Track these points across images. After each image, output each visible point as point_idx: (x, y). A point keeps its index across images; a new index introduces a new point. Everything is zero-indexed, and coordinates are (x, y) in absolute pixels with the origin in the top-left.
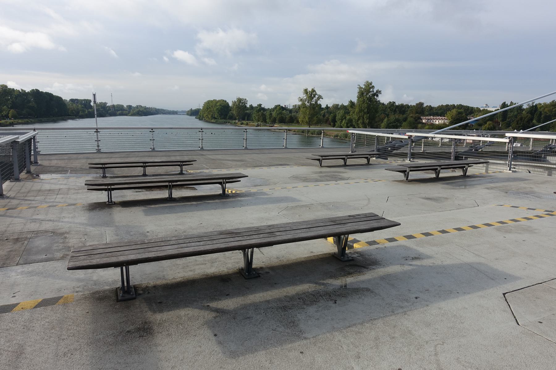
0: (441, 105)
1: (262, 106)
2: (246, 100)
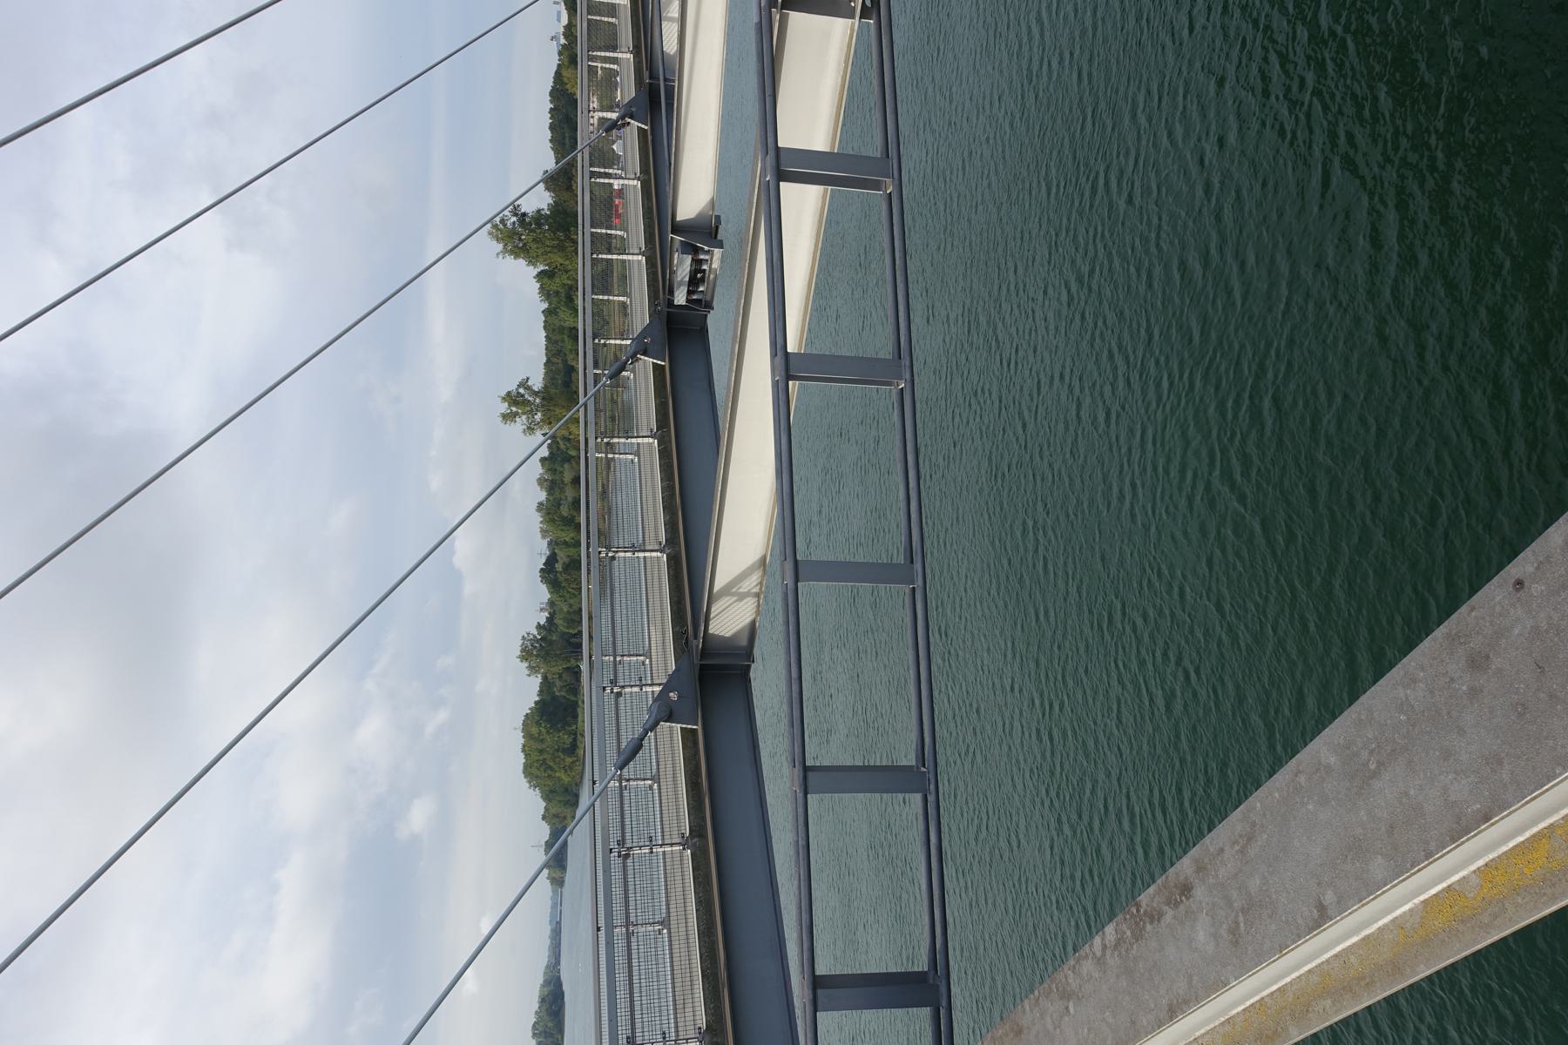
0: (550, 145)
1: (542, 623)
2: (526, 635)
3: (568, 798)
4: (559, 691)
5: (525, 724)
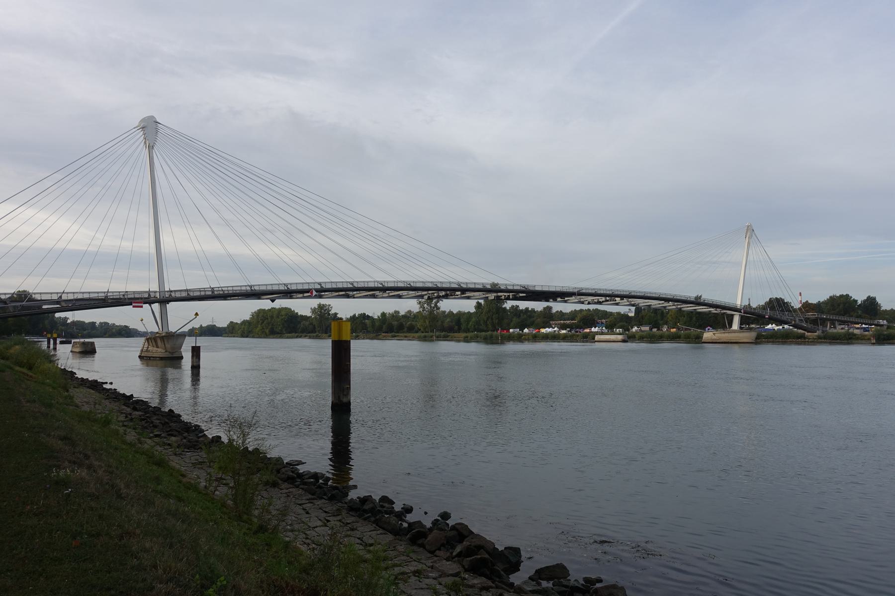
0: (573, 310)
3: (246, 332)
4: (303, 324)
5: (286, 308)
